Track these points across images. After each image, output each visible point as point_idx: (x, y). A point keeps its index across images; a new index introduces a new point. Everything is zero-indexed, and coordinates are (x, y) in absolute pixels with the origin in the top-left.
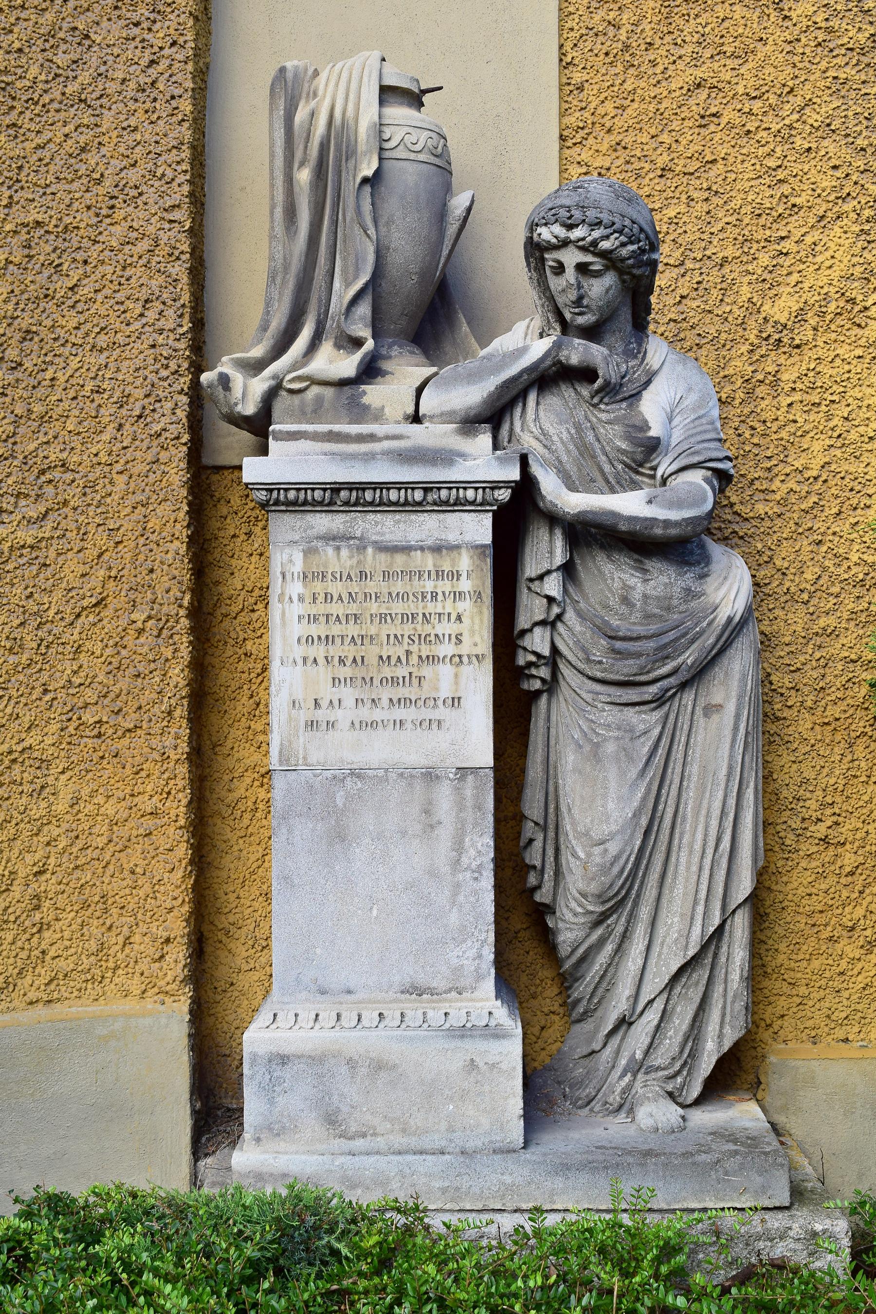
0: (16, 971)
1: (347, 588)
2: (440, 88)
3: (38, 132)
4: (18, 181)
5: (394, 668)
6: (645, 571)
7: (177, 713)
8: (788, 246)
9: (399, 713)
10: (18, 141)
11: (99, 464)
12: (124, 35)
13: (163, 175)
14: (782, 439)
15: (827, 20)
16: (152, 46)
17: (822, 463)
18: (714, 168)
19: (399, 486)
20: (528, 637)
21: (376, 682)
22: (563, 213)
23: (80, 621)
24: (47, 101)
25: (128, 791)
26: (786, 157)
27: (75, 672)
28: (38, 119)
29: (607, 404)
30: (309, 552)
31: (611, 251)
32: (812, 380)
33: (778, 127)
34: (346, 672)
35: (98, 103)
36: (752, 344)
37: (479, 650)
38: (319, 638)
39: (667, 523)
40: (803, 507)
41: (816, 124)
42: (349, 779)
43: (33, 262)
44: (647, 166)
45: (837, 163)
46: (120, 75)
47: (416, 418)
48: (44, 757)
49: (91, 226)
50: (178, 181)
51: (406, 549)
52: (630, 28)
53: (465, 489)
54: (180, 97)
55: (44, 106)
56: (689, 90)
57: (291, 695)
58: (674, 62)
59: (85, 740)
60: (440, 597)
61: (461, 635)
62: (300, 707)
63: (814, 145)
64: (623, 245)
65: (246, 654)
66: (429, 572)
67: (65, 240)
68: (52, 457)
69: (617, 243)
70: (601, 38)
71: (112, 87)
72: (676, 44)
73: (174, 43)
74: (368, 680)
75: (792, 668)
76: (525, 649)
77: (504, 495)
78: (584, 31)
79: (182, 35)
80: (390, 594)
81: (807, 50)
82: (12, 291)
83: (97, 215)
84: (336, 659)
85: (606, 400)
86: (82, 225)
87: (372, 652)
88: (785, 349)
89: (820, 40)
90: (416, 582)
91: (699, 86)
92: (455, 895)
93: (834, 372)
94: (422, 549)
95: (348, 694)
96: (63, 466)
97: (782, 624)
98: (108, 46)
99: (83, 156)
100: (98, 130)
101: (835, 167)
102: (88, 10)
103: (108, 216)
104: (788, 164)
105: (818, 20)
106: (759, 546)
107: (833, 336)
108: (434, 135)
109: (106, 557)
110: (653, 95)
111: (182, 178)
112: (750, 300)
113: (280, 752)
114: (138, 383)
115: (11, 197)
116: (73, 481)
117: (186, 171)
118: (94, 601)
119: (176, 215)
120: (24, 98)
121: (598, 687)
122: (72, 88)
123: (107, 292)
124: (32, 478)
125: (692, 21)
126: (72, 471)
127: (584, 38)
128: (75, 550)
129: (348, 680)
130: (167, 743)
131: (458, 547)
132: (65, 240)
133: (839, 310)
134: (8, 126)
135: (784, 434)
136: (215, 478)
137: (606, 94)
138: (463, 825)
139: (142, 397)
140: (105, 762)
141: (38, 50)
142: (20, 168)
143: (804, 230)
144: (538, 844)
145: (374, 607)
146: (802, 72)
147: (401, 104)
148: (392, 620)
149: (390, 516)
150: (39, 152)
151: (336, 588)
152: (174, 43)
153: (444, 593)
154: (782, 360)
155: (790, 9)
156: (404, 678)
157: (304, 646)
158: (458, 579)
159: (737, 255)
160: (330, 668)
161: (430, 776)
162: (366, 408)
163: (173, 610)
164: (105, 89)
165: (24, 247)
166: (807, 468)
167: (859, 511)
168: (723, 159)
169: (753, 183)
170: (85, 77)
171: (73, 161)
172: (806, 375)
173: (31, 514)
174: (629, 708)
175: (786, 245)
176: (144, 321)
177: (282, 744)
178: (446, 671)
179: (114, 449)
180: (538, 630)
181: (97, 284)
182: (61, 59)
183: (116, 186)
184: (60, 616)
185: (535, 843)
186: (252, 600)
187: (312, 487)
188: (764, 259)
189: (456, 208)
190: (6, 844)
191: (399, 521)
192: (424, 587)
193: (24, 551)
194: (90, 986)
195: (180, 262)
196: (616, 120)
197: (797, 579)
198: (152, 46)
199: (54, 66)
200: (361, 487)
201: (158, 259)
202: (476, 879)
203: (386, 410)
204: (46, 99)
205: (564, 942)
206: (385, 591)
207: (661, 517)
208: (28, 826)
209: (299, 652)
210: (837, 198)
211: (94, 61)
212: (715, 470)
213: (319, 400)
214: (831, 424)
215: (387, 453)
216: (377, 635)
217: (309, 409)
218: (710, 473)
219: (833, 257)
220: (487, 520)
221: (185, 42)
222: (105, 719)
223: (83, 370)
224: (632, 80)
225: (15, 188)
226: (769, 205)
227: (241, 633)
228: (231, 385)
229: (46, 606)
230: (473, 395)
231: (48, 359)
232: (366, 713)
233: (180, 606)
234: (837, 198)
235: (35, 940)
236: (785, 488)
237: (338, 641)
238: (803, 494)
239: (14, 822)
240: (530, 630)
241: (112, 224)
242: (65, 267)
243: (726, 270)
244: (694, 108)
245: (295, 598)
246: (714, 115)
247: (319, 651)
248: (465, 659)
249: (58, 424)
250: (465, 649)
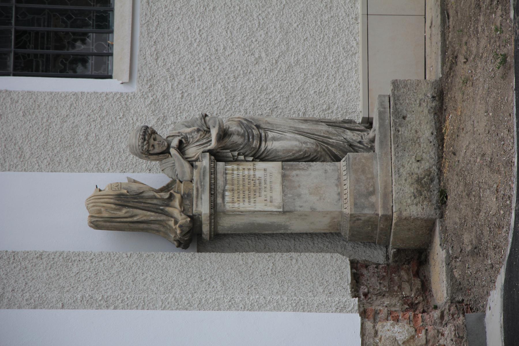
9: (268, 183)
34: (258, 194)
91: (87, 139)
95: (263, 193)
145: (241, 187)
209: (252, 204)
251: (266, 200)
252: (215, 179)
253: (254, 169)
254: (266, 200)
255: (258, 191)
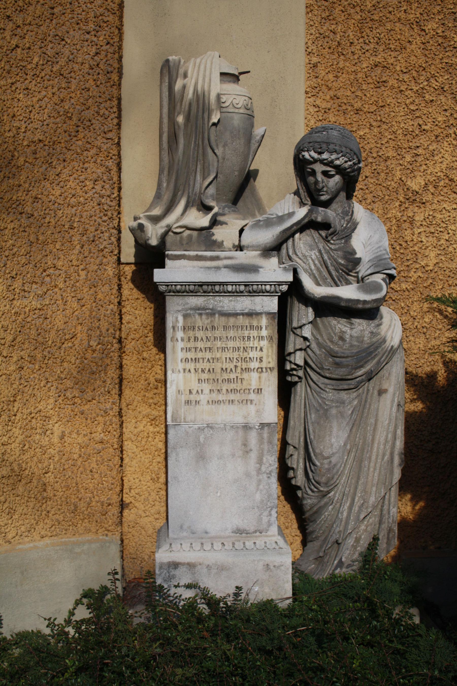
0: (35, 522)
1: (205, 334)
2: (249, 72)
3: (39, 92)
4: (30, 118)
5: (229, 374)
6: (352, 324)
7: (113, 392)
8: (420, 151)
9: (232, 396)
10: (29, 96)
11: (73, 266)
12: (82, 39)
13: (104, 114)
14: (415, 251)
15: (443, 32)
16: (97, 45)
17: (435, 263)
18: (384, 109)
19: (232, 284)
20: (293, 355)
21: (220, 381)
22: (317, 146)
23: (64, 346)
24: (43, 75)
25: (89, 431)
26: (420, 104)
27: (61, 372)
28: (39, 85)
29: (334, 240)
30: (185, 316)
31: (340, 166)
32: (431, 220)
33: (417, 88)
34: (205, 376)
35: (69, 75)
36: (401, 202)
37: (271, 365)
38: (192, 359)
39: (365, 302)
40: (425, 285)
41: (436, 87)
42: (206, 429)
43: (37, 161)
44: (350, 108)
45: (447, 108)
46: (80, 60)
47: (240, 248)
48: (47, 415)
49: (67, 142)
50: (111, 117)
51: (236, 315)
52: (342, 34)
53: (265, 285)
54: (112, 72)
55: (42, 78)
56: (372, 68)
57: (177, 387)
58: (364, 53)
59: (67, 406)
60: (252, 339)
61: (262, 357)
62: (182, 394)
63: (434, 99)
64: (346, 162)
65: (143, 359)
66: (247, 326)
67: (53, 149)
68: (50, 263)
69: (343, 161)
70: (326, 39)
71: (76, 67)
72: (365, 43)
73: (108, 43)
74: (216, 380)
75: (418, 366)
76: (291, 362)
77: (285, 288)
78: (318, 35)
79: (112, 39)
80: (227, 337)
81: (433, 48)
82: (28, 177)
83: (70, 136)
84: (200, 370)
85: (334, 238)
86: (62, 141)
87: (218, 366)
88: (417, 204)
89: (440, 42)
90: (240, 331)
91: (376, 66)
92: (258, 485)
93: (442, 216)
94: (243, 314)
95: (206, 387)
96: (55, 267)
97: (413, 344)
98: (74, 45)
99: (62, 104)
100: (69, 90)
101: (446, 110)
102: (63, 25)
103: (76, 136)
104: (422, 108)
105: (439, 32)
106: (403, 305)
107: (442, 198)
108: (247, 98)
109: (76, 313)
110: (353, 70)
111: (113, 116)
112: (400, 179)
113: (172, 416)
114: (92, 223)
115: (26, 127)
116: (60, 275)
117: (115, 112)
118: (71, 336)
119: (110, 135)
120: (32, 74)
121: (326, 381)
122: (56, 68)
123: (75, 176)
124: (39, 274)
125: (374, 31)
126: (59, 269)
127: (318, 39)
128: (61, 310)
129: (206, 381)
130: (108, 407)
131: (261, 314)
132: (53, 149)
133: (445, 185)
134: (24, 89)
135: (416, 248)
136: (414, 503)
137: (329, 69)
138: (263, 451)
139: (93, 230)
140: (77, 417)
141: (38, 47)
142: (31, 112)
143: (429, 143)
144: (295, 457)
145: (219, 344)
146: (430, 59)
147: (230, 82)
148: (228, 350)
149: (227, 298)
150: (40, 102)
151: (200, 334)
152: (108, 43)
153: (254, 337)
154: (416, 209)
155: (424, 25)
156: (234, 379)
157: (184, 363)
158: (261, 330)
159: (395, 155)
160: (197, 374)
161: (246, 427)
162: (215, 242)
163: (111, 339)
164: (73, 68)
165: (34, 154)
166: (427, 266)
167: (452, 287)
168: (388, 105)
169: (403, 118)
170: (62, 62)
171: (57, 107)
172: (428, 218)
173: (39, 292)
174: (342, 391)
175: (420, 151)
176: (94, 191)
177: (173, 412)
178: (255, 375)
179: (80, 258)
180: (298, 353)
181: (70, 172)
182: (50, 52)
183: (79, 120)
184: (54, 344)
185: (293, 456)
186: (146, 331)
187: (189, 284)
188: (408, 158)
189: (257, 136)
190: (29, 460)
191: (231, 301)
192: (244, 334)
193: (36, 311)
194: (71, 528)
195: (113, 160)
196: (334, 83)
197: (421, 322)
198: (97, 45)
199: (46, 56)
200: (214, 284)
201: (101, 159)
202: (269, 477)
203: (224, 243)
204: (43, 74)
205: (307, 504)
206: (225, 336)
207: (361, 299)
208: (40, 450)
209: (181, 366)
210: (446, 126)
211: (67, 53)
212: (388, 274)
213: (190, 236)
214: (439, 243)
215: (226, 267)
216: (221, 358)
217: (185, 242)
218: (385, 276)
219: (443, 157)
220: (275, 300)
221: (114, 43)
222: (77, 395)
223: (64, 217)
224: (342, 62)
225: (28, 122)
226: (411, 130)
227: (141, 348)
228: (145, 229)
229: (48, 339)
230: (268, 236)
231: (46, 212)
232: (215, 396)
233: (114, 338)
234: (446, 126)
235: (44, 506)
236: (416, 276)
237: (201, 361)
238: (425, 278)
239: (33, 448)
240: (294, 353)
241: (77, 140)
242: (54, 164)
243: (389, 163)
244: (374, 78)
245: (179, 339)
246: (384, 82)
247: (191, 366)
248: (264, 370)
249: (52, 245)
250: (264, 365)
251: (190, 392)
252: (238, 293)
253: (260, 370)
254: (190, 392)
255: (211, 376)
